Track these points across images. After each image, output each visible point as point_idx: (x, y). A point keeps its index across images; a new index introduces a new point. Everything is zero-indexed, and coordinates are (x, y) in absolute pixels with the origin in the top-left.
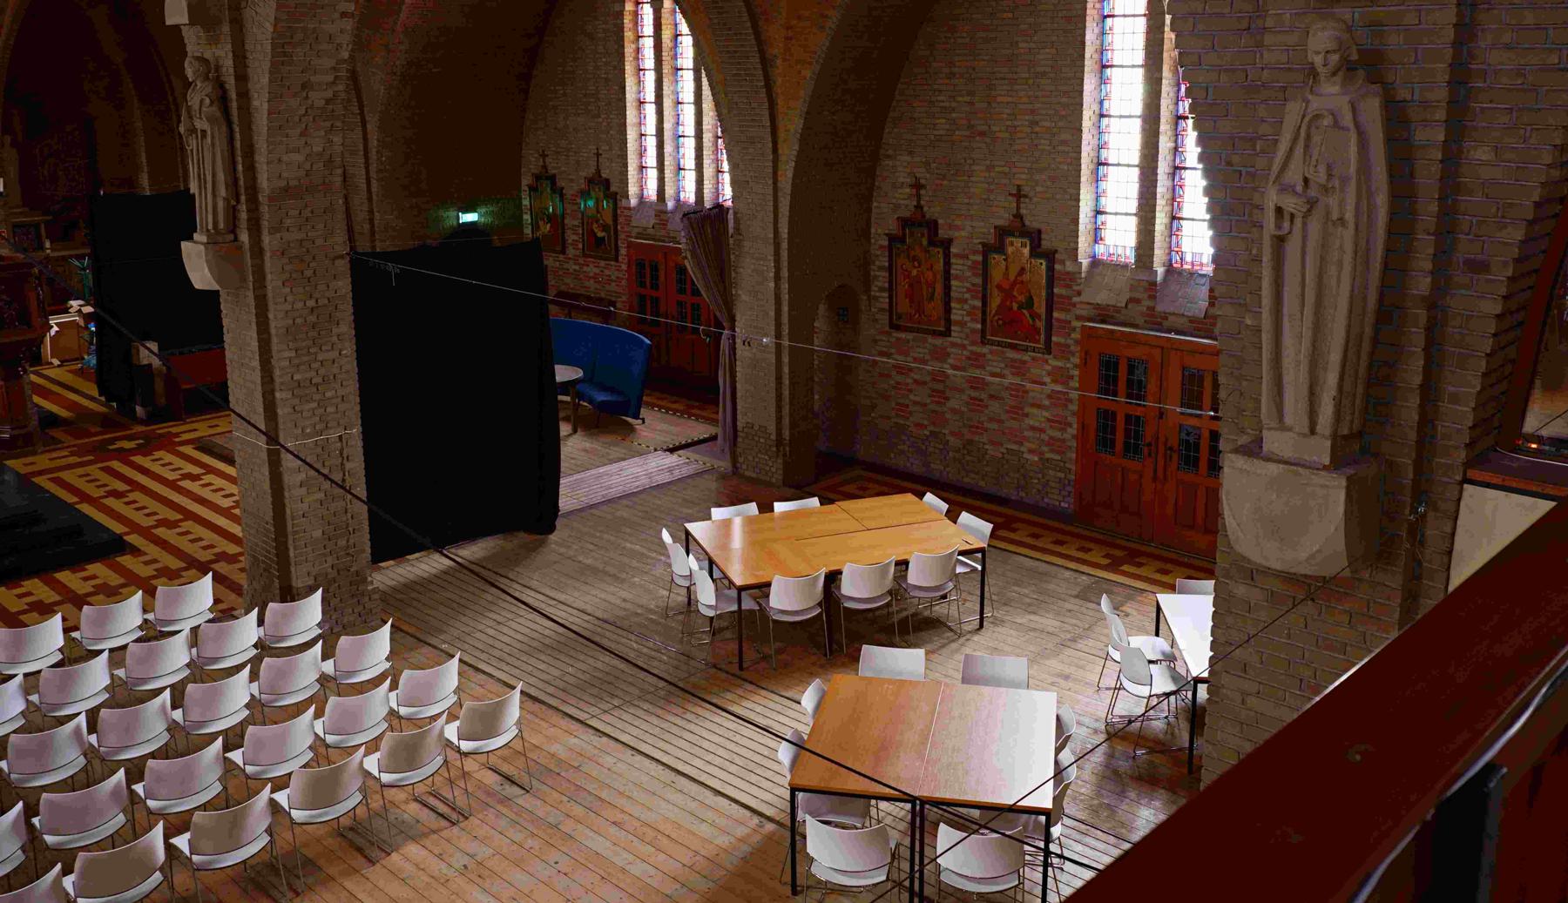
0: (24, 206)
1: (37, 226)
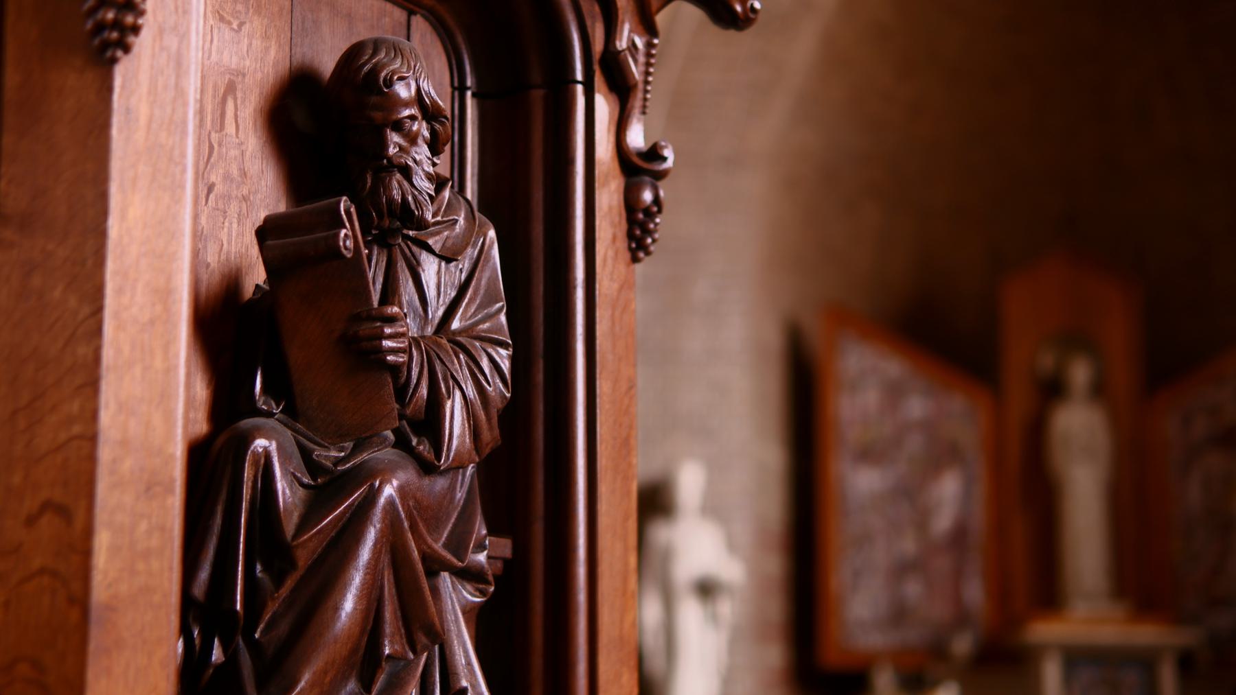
1: (1145, 661)
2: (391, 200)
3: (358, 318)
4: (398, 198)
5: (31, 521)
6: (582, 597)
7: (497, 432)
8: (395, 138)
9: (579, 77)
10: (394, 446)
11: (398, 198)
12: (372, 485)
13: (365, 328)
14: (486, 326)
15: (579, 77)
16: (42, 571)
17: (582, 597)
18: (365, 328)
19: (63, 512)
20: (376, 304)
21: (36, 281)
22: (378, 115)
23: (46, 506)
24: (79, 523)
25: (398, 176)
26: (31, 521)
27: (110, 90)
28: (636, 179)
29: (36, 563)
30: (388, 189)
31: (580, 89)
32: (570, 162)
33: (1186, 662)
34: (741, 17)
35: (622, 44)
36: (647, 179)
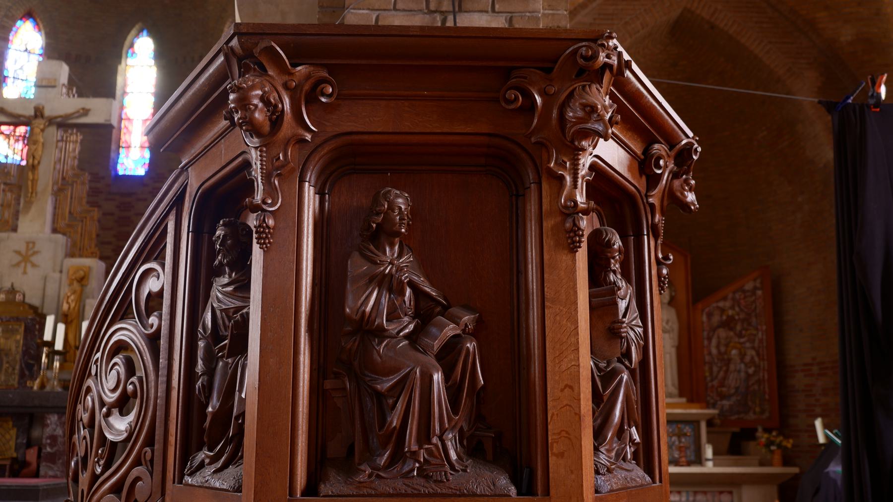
0: (681, 395)
1: (694, 423)
2: (611, 281)
3: (614, 322)
4: (613, 280)
5: (562, 390)
6: (654, 409)
7: (642, 356)
8: (612, 261)
9: (645, 233)
10: (617, 362)
11: (613, 280)
12: (622, 376)
13: (616, 325)
14: (635, 321)
15: (645, 233)
16: (567, 405)
17: (654, 409)
18: (616, 325)
19: (571, 387)
20: (620, 317)
21: (558, 318)
22: (609, 254)
23: (566, 386)
24: (576, 391)
25: (612, 274)
26: (562, 390)
27: (165, 103)
28: (660, 266)
29: (565, 403)
30: (609, 278)
31: (646, 237)
32: (644, 262)
33: (710, 423)
34: (693, 211)
35: (657, 220)
36: (664, 266)
